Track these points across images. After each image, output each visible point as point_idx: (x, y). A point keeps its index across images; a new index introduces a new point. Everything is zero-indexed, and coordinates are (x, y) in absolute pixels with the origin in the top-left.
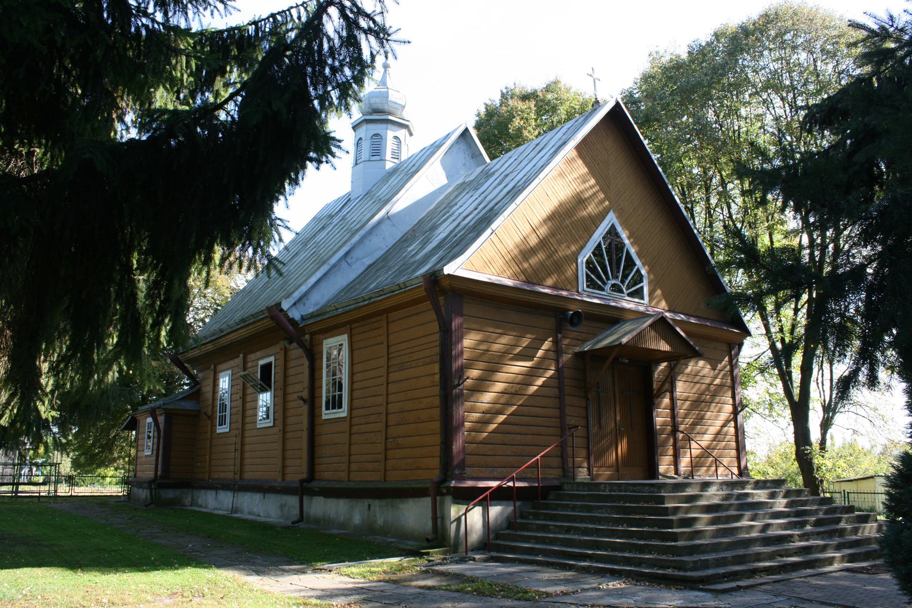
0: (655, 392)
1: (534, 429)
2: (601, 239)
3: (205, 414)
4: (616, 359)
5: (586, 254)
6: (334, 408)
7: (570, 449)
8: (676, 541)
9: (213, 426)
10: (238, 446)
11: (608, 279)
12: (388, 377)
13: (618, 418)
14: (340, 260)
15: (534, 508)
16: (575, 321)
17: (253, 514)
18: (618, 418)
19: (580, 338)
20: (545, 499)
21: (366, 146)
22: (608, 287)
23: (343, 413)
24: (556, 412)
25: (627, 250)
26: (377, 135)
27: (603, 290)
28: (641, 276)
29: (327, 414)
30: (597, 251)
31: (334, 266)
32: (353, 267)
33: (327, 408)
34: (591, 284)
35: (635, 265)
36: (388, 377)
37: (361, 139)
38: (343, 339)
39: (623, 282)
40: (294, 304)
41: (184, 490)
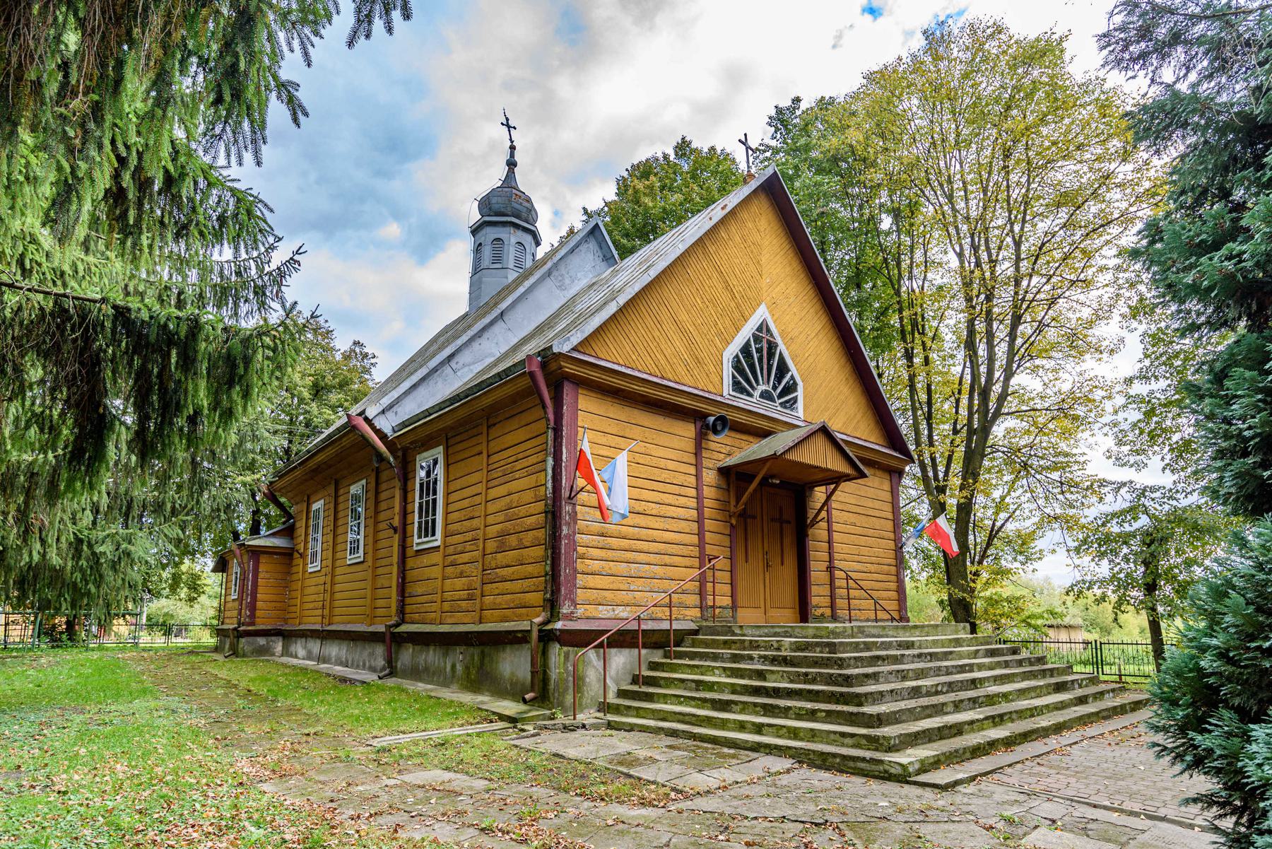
0: (809, 521)
1: (667, 559)
2: (731, 369)
3: (297, 551)
4: (764, 481)
5: (734, 348)
6: (426, 536)
7: (709, 585)
8: (860, 705)
9: (305, 565)
10: (328, 586)
11: (758, 383)
12: (486, 495)
13: (976, 402)
14: (442, 364)
15: (665, 657)
16: (719, 428)
17: (263, 661)
18: (976, 402)
19: (724, 451)
20: (679, 646)
21: (487, 252)
22: (757, 394)
23: (438, 540)
24: (695, 539)
25: (780, 352)
26: (499, 239)
27: (751, 396)
28: (795, 384)
29: (417, 542)
30: (746, 350)
31: (435, 370)
32: (459, 373)
33: (420, 537)
34: (737, 386)
35: (788, 370)
36: (486, 495)
37: (480, 244)
38: (438, 452)
39: (775, 388)
40: (383, 412)
41: (273, 638)
